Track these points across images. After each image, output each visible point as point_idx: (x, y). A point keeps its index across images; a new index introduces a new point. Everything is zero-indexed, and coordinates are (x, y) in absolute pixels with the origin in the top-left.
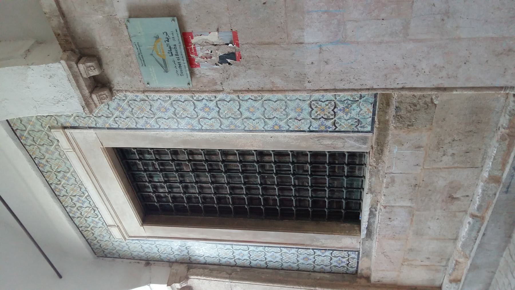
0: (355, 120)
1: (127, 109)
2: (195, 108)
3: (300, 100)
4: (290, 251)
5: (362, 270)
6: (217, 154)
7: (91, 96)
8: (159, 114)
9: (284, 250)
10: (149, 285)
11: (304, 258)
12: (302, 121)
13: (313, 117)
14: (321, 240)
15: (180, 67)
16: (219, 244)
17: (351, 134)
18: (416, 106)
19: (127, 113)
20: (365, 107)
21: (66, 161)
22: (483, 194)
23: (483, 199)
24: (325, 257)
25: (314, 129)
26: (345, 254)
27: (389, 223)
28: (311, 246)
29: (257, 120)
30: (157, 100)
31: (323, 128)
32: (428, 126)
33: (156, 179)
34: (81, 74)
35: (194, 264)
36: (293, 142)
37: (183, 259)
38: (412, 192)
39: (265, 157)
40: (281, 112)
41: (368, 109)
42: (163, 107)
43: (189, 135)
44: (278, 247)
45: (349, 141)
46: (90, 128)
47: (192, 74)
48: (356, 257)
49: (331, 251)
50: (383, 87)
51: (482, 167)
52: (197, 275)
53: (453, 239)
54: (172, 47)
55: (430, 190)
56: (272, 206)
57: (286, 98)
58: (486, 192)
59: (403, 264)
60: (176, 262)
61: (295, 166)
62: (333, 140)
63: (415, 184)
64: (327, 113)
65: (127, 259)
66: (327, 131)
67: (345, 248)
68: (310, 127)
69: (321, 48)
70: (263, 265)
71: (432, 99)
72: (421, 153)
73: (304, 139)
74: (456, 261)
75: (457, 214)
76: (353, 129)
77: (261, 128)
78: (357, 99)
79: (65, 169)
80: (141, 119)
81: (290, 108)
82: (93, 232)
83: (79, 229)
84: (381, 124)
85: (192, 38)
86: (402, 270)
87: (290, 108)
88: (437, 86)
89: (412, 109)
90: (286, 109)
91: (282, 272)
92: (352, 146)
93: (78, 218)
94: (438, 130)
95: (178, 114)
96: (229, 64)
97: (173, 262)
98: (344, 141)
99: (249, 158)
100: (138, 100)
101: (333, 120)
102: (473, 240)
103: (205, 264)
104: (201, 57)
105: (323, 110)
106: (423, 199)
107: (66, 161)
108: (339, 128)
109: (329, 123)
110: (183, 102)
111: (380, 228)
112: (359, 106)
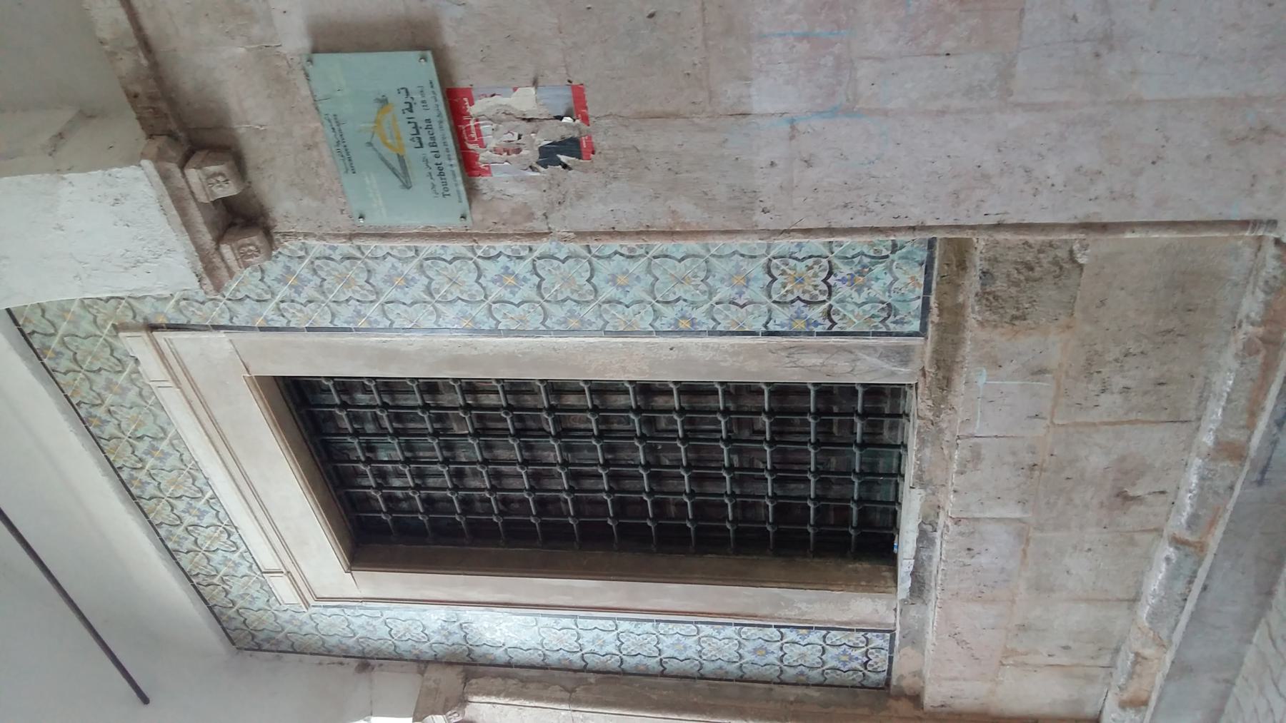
0: (881, 306)
1: (310, 281)
2: (479, 277)
3: (742, 255)
5: (901, 677)
7: (218, 249)
8: (390, 293)
11: (755, 651)
12: (749, 308)
13: (775, 297)
14: (799, 605)
15: (441, 174)
17: (871, 341)
19: (309, 291)
20: (905, 273)
22: (1201, 487)
25: (779, 329)
28: (773, 618)
29: (635, 307)
30: (384, 257)
32: (1063, 319)
34: (192, 193)
37: (454, 654)
39: (656, 399)
42: (399, 275)
43: (466, 345)
46: (217, 328)
47: (472, 191)
48: (886, 645)
49: (824, 632)
50: (950, 222)
52: (489, 694)
53: (1128, 600)
54: (422, 124)
63: (1031, 463)
64: (810, 288)
65: (311, 654)
66: (810, 334)
67: (858, 623)
68: (767, 323)
69: (793, 128)
71: (1071, 252)
72: (1045, 386)
73: (753, 352)
74: (1137, 654)
84: (946, 315)
85: (472, 104)
89: (1022, 278)
90: (707, 277)
91: (701, 684)
94: (1088, 328)
96: (565, 166)
98: (853, 357)
101: (825, 306)
102: (1177, 601)
103: (508, 665)
104: (495, 150)
105: (800, 280)
106: (1052, 501)
108: (840, 324)
109: (816, 313)
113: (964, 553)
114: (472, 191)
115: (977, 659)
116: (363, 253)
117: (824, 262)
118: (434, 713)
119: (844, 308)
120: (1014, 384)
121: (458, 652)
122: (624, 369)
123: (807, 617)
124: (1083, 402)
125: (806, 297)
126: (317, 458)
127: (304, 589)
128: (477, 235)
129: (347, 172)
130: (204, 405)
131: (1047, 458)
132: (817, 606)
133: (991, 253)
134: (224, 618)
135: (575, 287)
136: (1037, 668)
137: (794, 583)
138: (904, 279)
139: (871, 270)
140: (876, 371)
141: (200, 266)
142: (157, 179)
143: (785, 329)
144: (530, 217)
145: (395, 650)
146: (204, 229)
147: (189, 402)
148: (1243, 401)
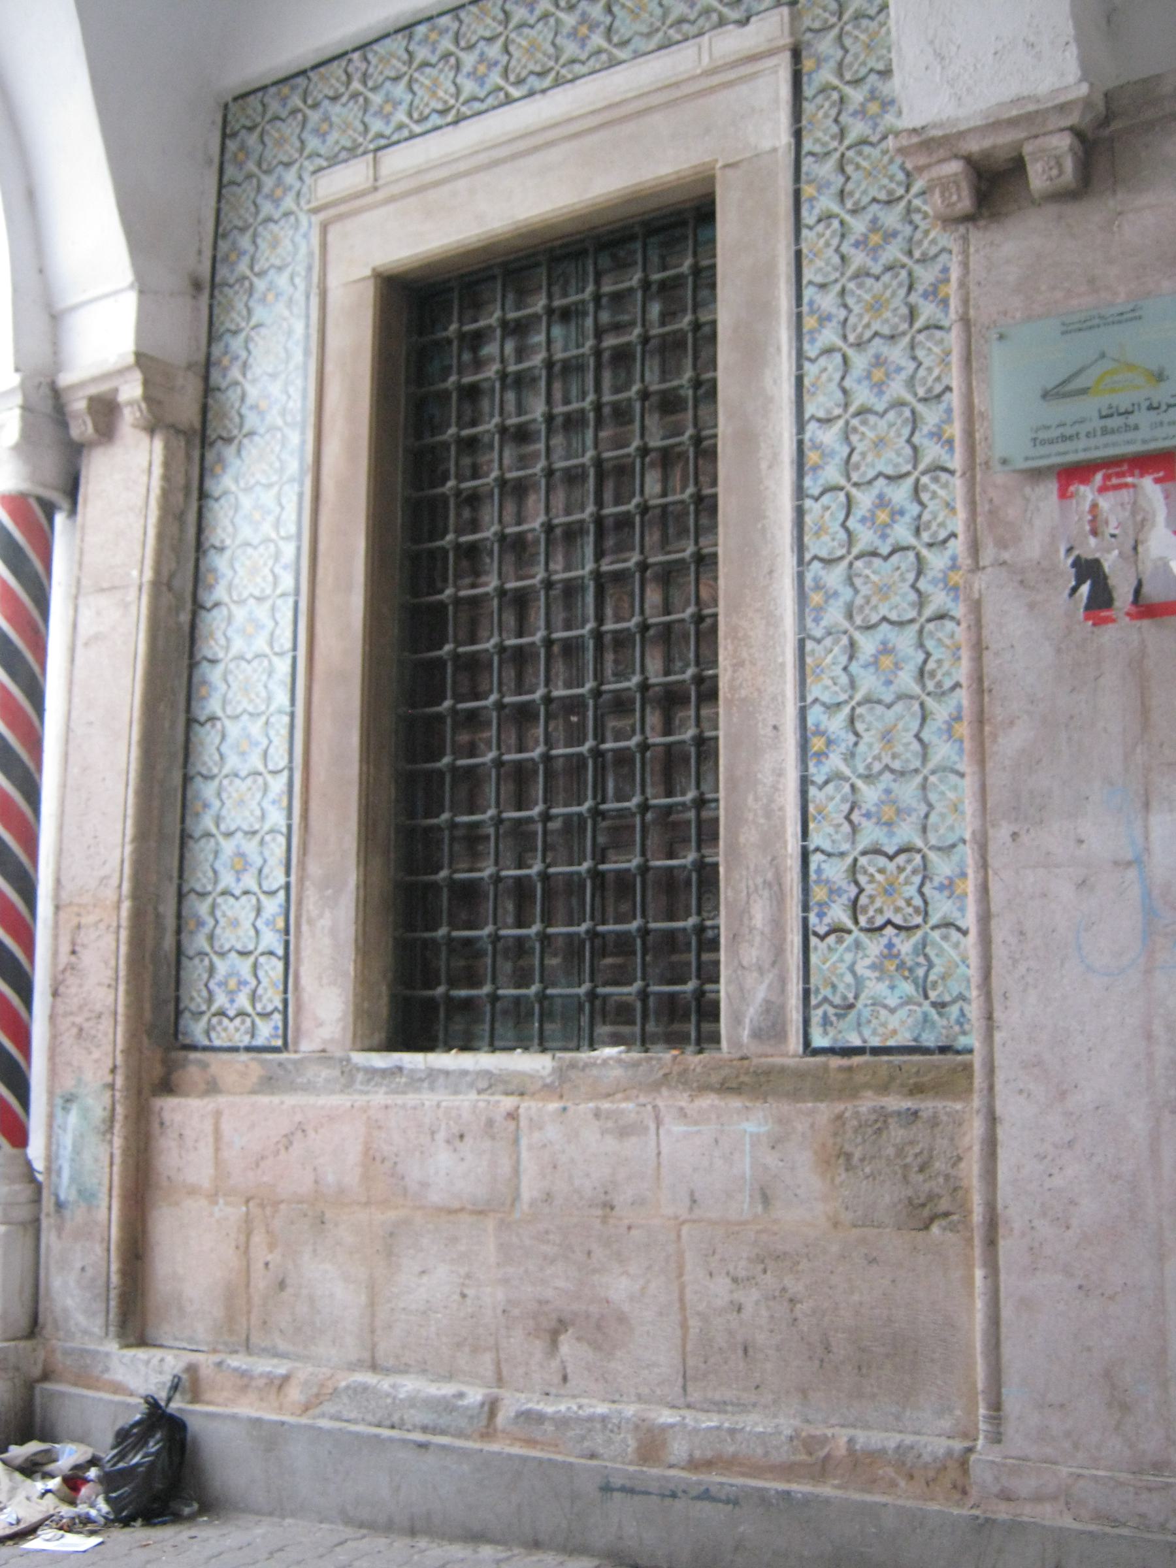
0: (851, 996)
1: (875, 259)
2: (888, 477)
3: (927, 816)
4: (274, 802)
5: (205, 1066)
6: (668, 548)
7: (956, 156)
8: (860, 362)
9: (278, 785)
10: (131, 287)
11: (241, 855)
12: (846, 828)
13: (863, 861)
14: (327, 914)
15: (1064, 438)
16: (299, 549)
17: (795, 988)
18: (921, 1170)
19: (859, 258)
20: (903, 1022)
21: (657, 38)
22: (591, 1419)
23: (563, 1422)
24: (252, 933)
25: (813, 867)
26: (271, 1000)
27: (441, 1136)
28: (301, 880)
29: (844, 679)
30: (914, 358)
31: (819, 893)
32: (846, 1217)
33: (557, 331)
34: (1036, 137)
35: (202, 458)
36: (756, 799)
37: (223, 415)
38: (581, 1198)
39: (657, 713)
40: (878, 758)
41: (895, 1032)
42: (887, 375)
43: (776, 456)
44: (291, 760)
45: (767, 982)
46: (798, 135)
47: (1036, 474)
48: (259, 1041)
49: (280, 952)
50: (1000, 1059)
51: (689, 1406)
52: (167, 464)
53: (373, 1358)
54: (1132, 420)
55: (589, 1253)
56: (453, 742)
57: (933, 772)
58: (598, 1426)
59: (251, 1204)
60: (208, 390)
61: (633, 815)
62: (767, 930)
63: (615, 1203)
64: (878, 904)
65: (218, 211)
66: (806, 908)
67: (298, 999)
68: (823, 852)
69: (1129, 864)
70: (203, 708)
71: (946, 1214)
72: (744, 1206)
73: (775, 835)
74: (286, 1378)
75: (488, 1358)
76: (817, 991)
77: (814, 691)
78: (933, 995)
79: (625, 26)
80: (839, 301)
81: (894, 786)
82: (344, 99)
83: (355, 50)
84: (841, 1076)
85: (1157, 481)
86: (221, 1201)
87: (894, 786)
88: (1001, 1222)
89: (909, 1160)
90: (892, 771)
91: (177, 778)
92: (743, 993)
93: (407, 50)
94: (835, 1249)
95: (864, 423)
96: (1074, 590)
97: (206, 378)
98: (767, 966)
99: (653, 658)
100: (914, 298)
101: (849, 924)
102: (390, 1415)
103: (203, 495)
104: (1094, 506)
105: (889, 890)
106: (551, 1237)
107: (657, 38)
108: (822, 946)
109: (839, 913)
110: (909, 441)
111: (415, 1108)
112: (908, 1001)
113: (455, 1130)
114: (1036, 474)
115: (257, 1165)
116: (920, 331)
117: (918, 920)
118: (146, 383)
119: (848, 949)
120: (745, 1165)
121: (227, 422)
122: (739, 665)
123: (305, 928)
124: (717, 1257)
125: (863, 900)
126: (559, 242)
127: (343, 208)
128: (973, 477)
129: (1063, 324)
130: (667, 104)
131: (626, 1222)
132: (327, 941)
133: (945, 1118)
134: (285, 90)
135: (874, 600)
136: (245, 1250)
137: (364, 904)
138: (894, 1022)
139: (906, 978)
140: (743, 998)
141: (938, 133)
142: (1062, 99)
143: (813, 876)
144: (1002, 544)
145: (228, 330)
146: (987, 143)
147: (677, 84)
148: (731, 1449)
